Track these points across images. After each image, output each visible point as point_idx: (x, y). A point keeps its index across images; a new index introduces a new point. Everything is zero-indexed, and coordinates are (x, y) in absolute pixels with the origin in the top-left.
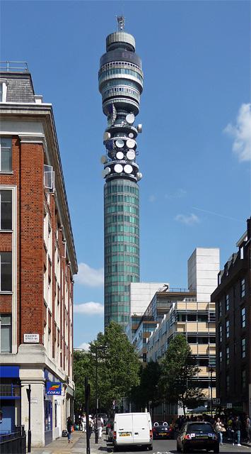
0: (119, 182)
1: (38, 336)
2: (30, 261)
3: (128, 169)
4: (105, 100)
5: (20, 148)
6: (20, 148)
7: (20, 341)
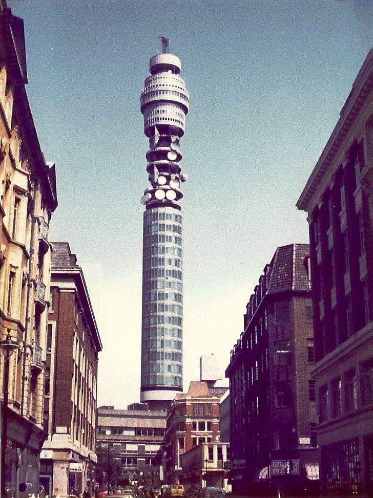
0: (161, 210)
1: (66, 428)
3: (171, 196)
4: (146, 123)
5: (59, 294)
6: (59, 294)
7: (54, 432)
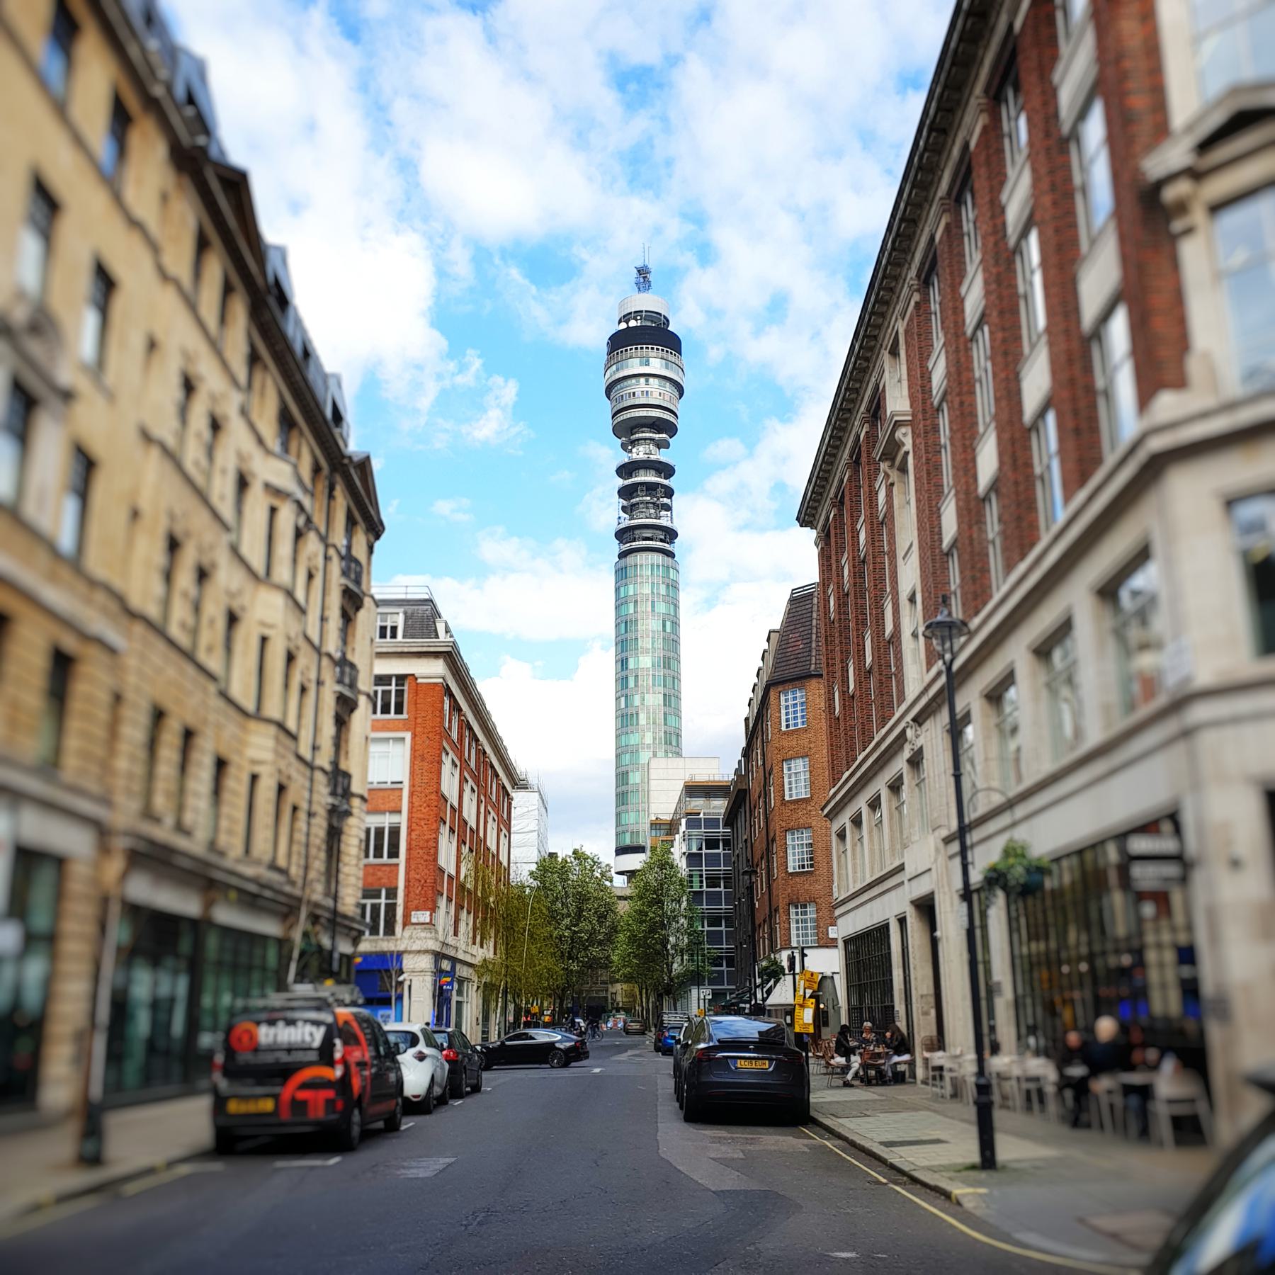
1: (428, 913)
2: (422, 823)
